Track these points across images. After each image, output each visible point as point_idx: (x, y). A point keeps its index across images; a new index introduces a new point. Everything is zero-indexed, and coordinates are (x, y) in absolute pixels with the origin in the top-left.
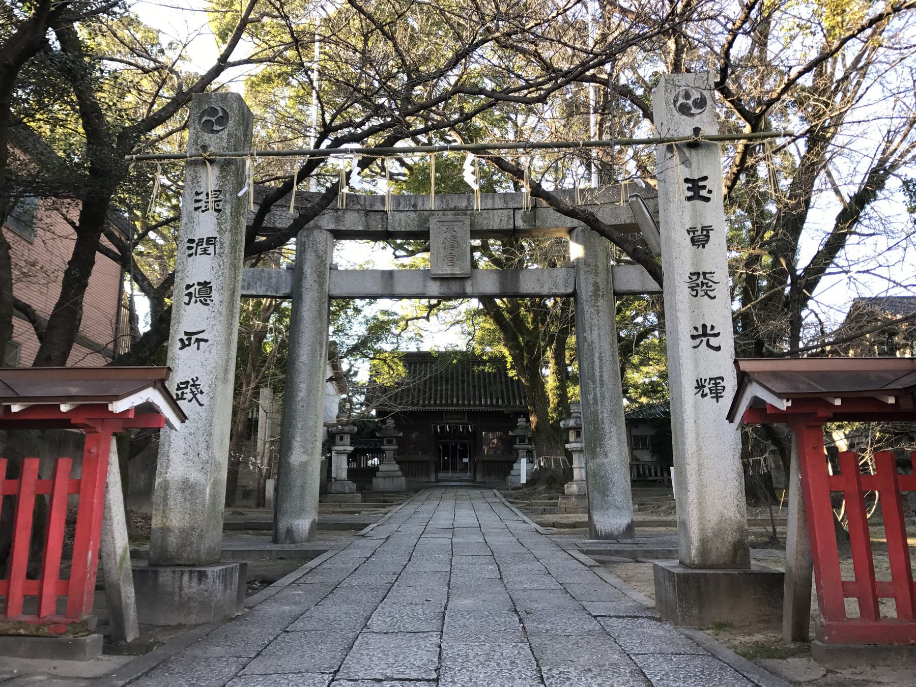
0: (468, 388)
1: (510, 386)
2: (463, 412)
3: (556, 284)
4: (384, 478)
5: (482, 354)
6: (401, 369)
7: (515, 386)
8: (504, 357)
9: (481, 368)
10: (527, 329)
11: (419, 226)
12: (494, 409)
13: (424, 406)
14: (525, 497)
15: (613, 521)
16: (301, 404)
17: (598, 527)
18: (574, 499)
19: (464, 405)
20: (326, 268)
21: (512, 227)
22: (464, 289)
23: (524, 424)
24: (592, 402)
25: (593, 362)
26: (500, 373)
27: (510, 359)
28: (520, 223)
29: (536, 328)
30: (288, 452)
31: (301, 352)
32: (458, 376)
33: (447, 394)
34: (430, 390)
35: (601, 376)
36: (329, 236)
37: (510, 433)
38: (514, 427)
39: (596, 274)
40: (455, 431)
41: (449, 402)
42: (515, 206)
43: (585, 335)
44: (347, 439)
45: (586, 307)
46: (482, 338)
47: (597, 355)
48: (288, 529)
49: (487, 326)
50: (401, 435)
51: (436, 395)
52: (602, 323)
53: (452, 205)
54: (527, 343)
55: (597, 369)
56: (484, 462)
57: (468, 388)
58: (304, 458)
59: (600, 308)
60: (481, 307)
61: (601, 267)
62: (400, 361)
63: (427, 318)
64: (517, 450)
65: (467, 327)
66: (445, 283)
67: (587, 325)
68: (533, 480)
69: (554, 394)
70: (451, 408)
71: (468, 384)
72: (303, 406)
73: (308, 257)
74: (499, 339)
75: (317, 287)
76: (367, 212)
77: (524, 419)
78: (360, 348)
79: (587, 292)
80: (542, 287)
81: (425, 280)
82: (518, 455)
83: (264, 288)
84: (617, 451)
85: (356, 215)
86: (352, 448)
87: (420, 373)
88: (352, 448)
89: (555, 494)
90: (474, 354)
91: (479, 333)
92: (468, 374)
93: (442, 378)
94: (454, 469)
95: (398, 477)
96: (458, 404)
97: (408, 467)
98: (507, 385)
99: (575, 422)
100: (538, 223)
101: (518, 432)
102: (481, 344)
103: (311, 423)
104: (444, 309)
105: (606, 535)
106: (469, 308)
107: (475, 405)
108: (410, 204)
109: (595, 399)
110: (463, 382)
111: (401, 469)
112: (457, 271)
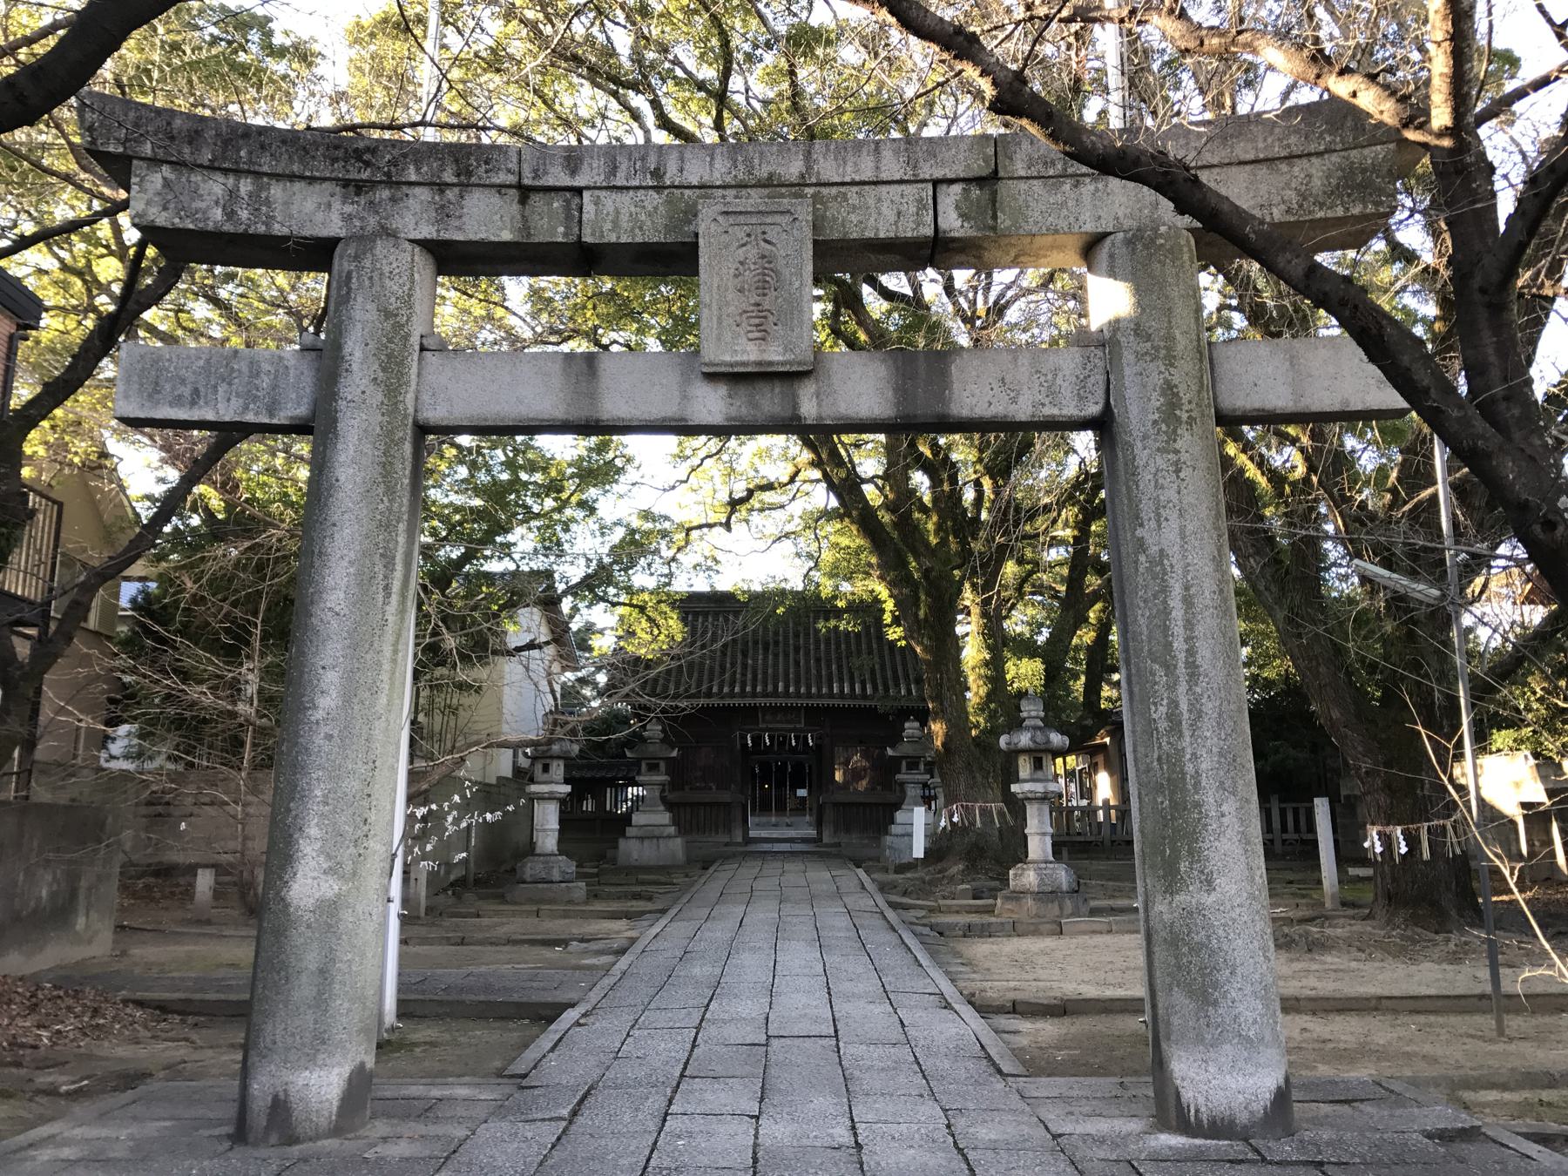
0: (807, 662)
1: (887, 658)
2: (797, 709)
3: (1052, 393)
4: (641, 839)
5: (835, 597)
6: (674, 625)
7: (898, 658)
8: (877, 600)
9: (832, 623)
10: (927, 544)
11: (668, 229)
12: (857, 703)
13: (720, 694)
14: (924, 889)
15: (1235, 1082)
16: (324, 730)
17: (1187, 1095)
18: (1030, 902)
19: (798, 695)
20: (402, 348)
21: (928, 231)
22: (796, 406)
23: (917, 733)
24: (1163, 725)
25: (1166, 612)
26: (868, 633)
27: (889, 605)
28: (952, 223)
29: (944, 542)
30: (283, 868)
31: (330, 582)
32: (786, 638)
33: (765, 673)
34: (733, 665)
35: (1191, 652)
36: (423, 264)
37: (890, 752)
38: (896, 738)
39: (1170, 361)
40: (782, 744)
41: (770, 688)
42: (939, 173)
43: (1139, 532)
44: (558, 770)
45: (1142, 455)
46: (835, 566)
47: (1177, 590)
48: (276, 1098)
49: (844, 541)
50: (675, 754)
51: (744, 675)
52: (1189, 499)
53: (763, 172)
54: (926, 573)
55: (1178, 630)
56: (836, 805)
57: (807, 662)
58: (330, 887)
59: (1184, 457)
60: (834, 502)
61: (1182, 343)
62: (673, 608)
63: (727, 525)
64: (902, 784)
65: (806, 543)
66: (743, 390)
67: (1146, 509)
68: (939, 849)
69: (980, 677)
70: (773, 701)
71: (807, 653)
72: (329, 737)
73: (358, 314)
74: (870, 565)
75: (380, 397)
76: (525, 193)
77: (917, 724)
78: (594, 584)
79: (1144, 411)
80: (1014, 401)
81: (686, 381)
82: (903, 792)
83: (236, 403)
84: (1239, 870)
85: (495, 199)
86: (568, 788)
87: (705, 632)
88: (568, 788)
89: (983, 882)
90: (818, 596)
91: (827, 556)
92: (807, 635)
93: (756, 643)
94: (781, 808)
95: (669, 837)
96: (787, 694)
97: (689, 814)
98: (882, 657)
99: (1033, 739)
100: (1004, 221)
101: (905, 749)
102: (831, 575)
103: (352, 785)
104: (762, 510)
105: (1213, 1122)
106: (809, 508)
107: (820, 695)
108: (644, 170)
109: (1173, 718)
110: (797, 649)
111: (675, 822)
112: (775, 355)
